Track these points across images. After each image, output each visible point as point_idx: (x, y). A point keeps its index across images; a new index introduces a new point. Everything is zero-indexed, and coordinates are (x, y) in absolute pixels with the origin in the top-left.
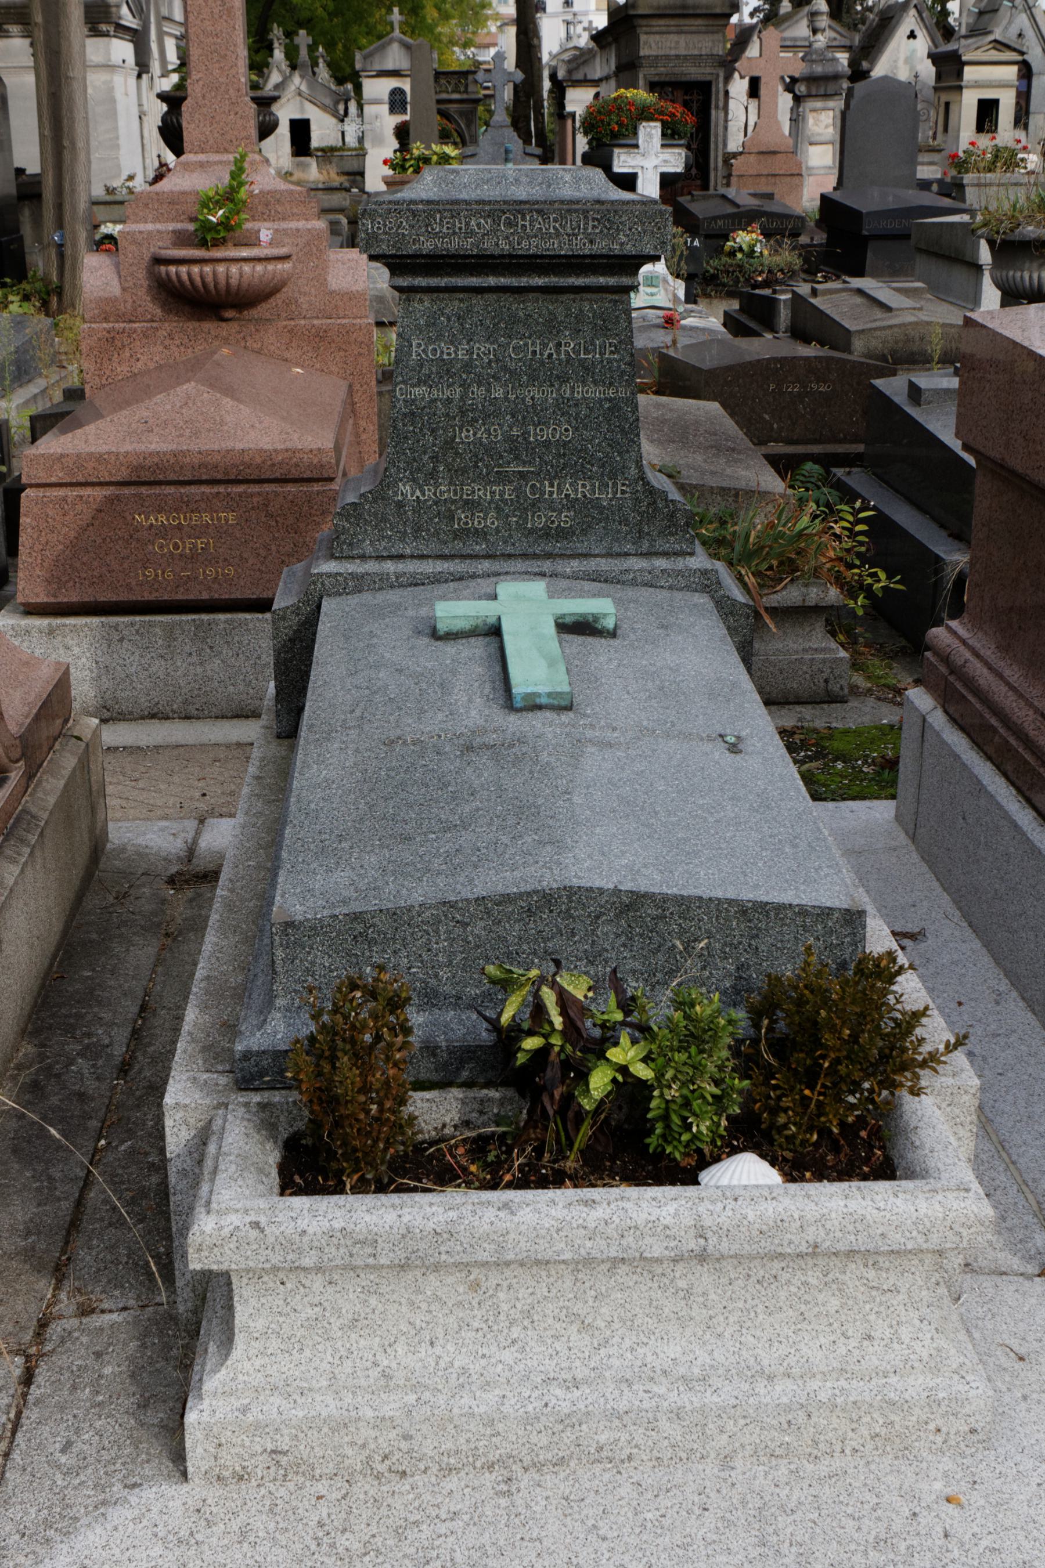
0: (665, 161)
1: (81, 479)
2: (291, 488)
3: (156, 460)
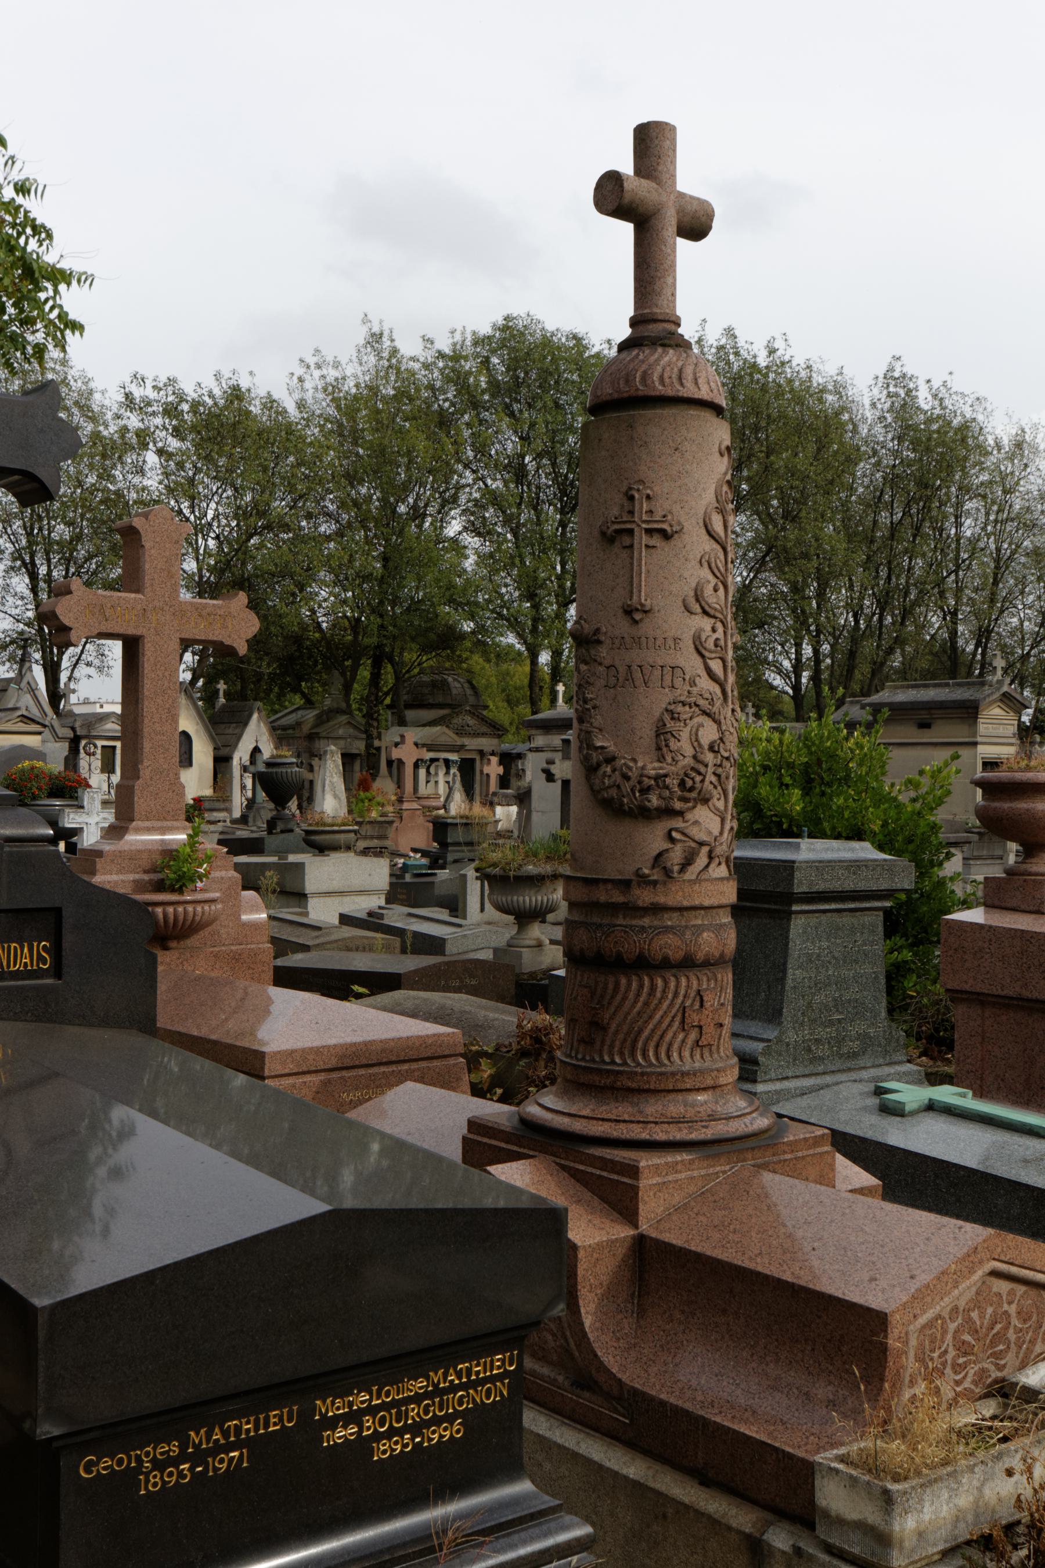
0: (105, 819)
1: (305, 1069)
2: (436, 1063)
3: (354, 1049)
